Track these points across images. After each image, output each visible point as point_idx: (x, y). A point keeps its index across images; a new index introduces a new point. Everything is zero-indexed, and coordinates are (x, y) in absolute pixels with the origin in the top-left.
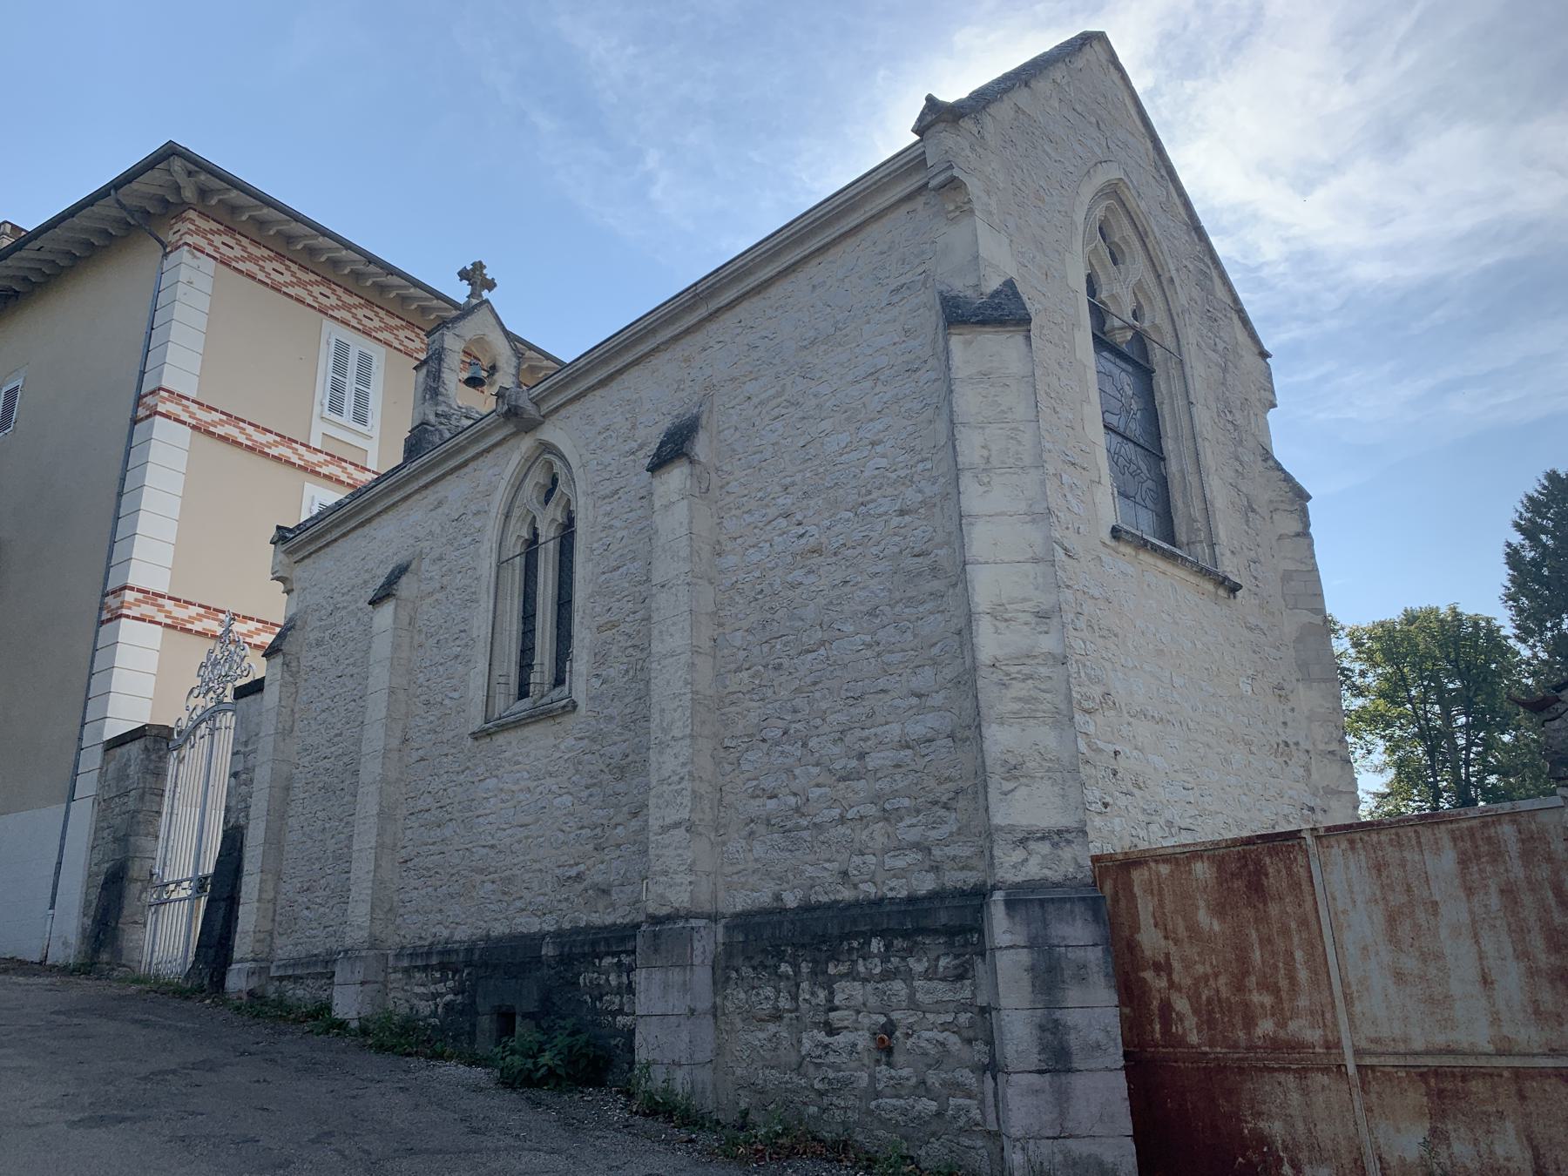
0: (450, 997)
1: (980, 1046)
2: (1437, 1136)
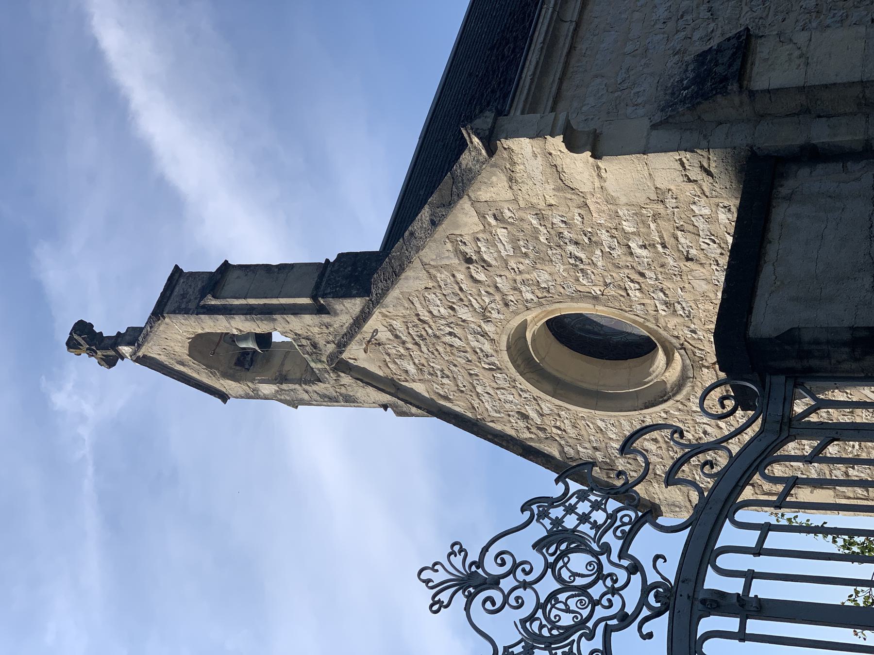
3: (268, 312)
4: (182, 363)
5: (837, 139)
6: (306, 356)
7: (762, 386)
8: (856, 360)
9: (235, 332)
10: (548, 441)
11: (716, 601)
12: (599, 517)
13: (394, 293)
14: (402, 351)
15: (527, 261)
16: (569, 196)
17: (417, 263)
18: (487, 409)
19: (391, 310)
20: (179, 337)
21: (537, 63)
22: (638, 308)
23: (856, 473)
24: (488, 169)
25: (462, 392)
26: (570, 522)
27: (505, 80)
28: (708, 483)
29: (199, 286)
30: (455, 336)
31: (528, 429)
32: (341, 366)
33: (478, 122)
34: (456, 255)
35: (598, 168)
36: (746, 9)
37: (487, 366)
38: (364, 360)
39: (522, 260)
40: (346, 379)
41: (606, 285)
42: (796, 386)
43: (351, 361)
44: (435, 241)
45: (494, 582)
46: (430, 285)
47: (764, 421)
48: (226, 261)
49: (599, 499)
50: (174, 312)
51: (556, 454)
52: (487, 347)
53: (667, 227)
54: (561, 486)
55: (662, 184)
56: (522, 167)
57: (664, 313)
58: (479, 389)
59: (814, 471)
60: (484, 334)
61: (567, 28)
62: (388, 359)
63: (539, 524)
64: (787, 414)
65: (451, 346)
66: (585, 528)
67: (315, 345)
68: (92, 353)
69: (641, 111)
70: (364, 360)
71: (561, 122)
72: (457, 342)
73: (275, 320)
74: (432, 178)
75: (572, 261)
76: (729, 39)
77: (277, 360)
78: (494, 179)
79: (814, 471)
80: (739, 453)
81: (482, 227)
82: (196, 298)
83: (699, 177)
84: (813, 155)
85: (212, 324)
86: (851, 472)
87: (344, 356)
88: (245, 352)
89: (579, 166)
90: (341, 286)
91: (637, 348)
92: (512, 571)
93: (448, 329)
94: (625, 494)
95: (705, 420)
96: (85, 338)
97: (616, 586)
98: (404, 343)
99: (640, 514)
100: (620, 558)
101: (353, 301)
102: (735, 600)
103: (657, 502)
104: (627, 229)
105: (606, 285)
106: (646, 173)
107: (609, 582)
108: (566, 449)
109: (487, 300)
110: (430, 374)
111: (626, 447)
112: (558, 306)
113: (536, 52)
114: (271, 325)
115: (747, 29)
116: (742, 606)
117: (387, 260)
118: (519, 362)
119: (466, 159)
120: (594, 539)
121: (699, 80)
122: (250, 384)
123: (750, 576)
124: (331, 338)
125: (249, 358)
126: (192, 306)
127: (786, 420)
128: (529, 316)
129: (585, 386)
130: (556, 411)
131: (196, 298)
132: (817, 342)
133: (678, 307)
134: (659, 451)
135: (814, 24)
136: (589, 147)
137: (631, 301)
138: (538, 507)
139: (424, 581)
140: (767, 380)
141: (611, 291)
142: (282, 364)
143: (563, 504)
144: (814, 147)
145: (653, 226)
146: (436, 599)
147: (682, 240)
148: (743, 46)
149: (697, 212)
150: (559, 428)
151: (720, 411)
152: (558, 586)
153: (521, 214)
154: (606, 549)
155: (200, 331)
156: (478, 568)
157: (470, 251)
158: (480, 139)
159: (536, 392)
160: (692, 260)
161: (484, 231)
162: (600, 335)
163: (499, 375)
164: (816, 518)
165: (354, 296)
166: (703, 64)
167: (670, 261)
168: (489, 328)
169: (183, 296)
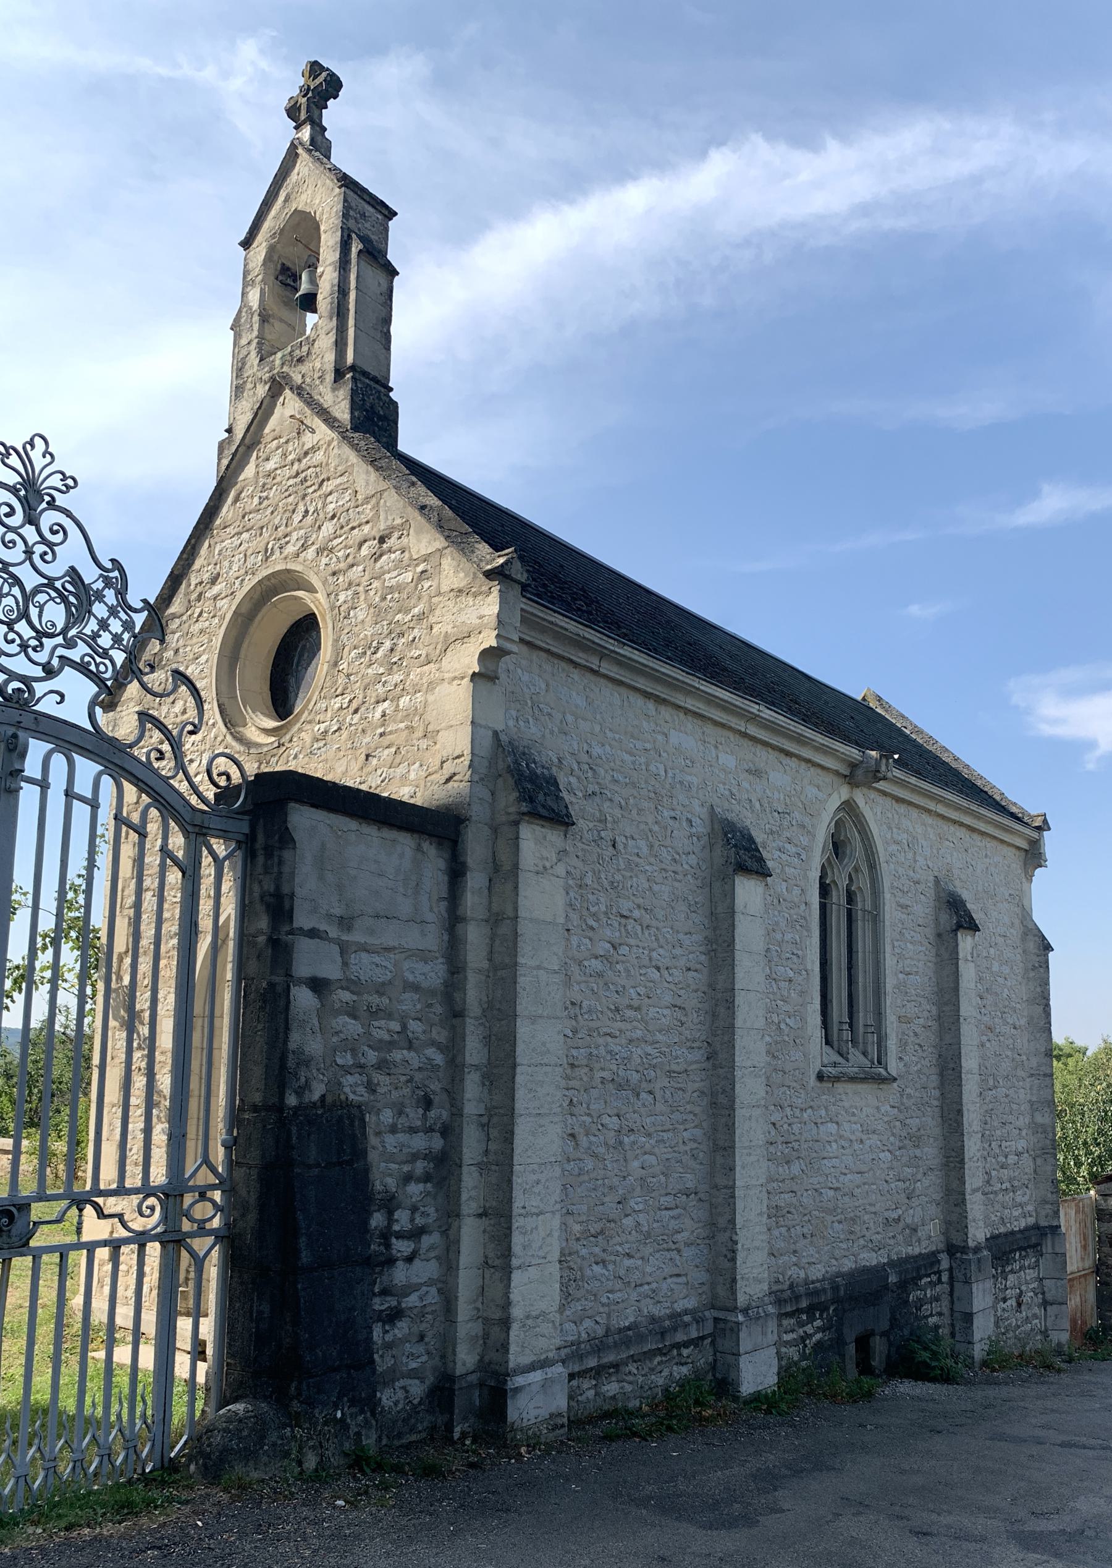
0: (819, 1336)
1: (1040, 1296)
2: (399, 1303)
3: (341, 312)
4: (287, 199)
5: (469, 895)
6: (289, 349)
7: (241, 812)
8: (262, 897)
9: (320, 270)
10: (186, 603)
11: (16, 748)
12: (105, 640)
13: (353, 457)
14: (291, 457)
15: (377, 599)
16: (439, 647)
17: (383, 485)
18: (221, 542)
19: (336, 451)
20: (317, 202)
21: (566, 630)
22: (323, 705)
23: (148, 898)
24: (473, 570)
25: (244, 517)
26: (100, 610)
27: (554, 598)
28: (140, 753)
29: (373, 237)
30: (304, 517)
31: (201, 583)
32: (277, 387)
33: (518, 565)
34: (388, 528)
35: (463, 678)
36: (591, 825)
37: (270, 546)
38: (282, 414)
39: (379, 594)
40: (262, 390)
41: (348, 676)
42: (239, 842)
43: (281, 399)
44: (405, 507)
45: (32, 519)
46: (359, 497)
47: (203, 812)
48: (398, 273)
49: (125, 643)
50: (345, 200)
51: (172, 610)
52: (290, 549)
53: (400, 739)
54: (140, 605)
55: (442, 737)
56: (471, 603)
57: (316, 729)
58: (245, 536)
59: (153, 860)
60: (304, 547)
61: (594, 662)
62: (282, 440)
63: (97, 577)
64: (211, 832)
65: (294, 511)
66: (92, 626)
67: (300, 360)
68: (305, 91)
69: (511, 723)
70: (282, 414)
71: (508, 646)
72: (297, 517)
73: (331, 319)
74: (470, 515)
75: (375, 644)
76: (566, 807)
77: (285, 314)
78: (462, 575)
79: (153, 860)
80: (172, 787)
81: (415, 557)
82: (359, 229)
83: (445, 771)
84: (456, 873)
85: (330, 243)
86: (150, 893)
87: (287, 392)
88: (296, 278)
89: (466, 659)
90: (364, 400)
91: (282, 699)
92: (44, 541)
93: (311, 509)
94: (131, 670)
95: (205, 762)
96: (322, 87)
97: (30, 650)
98: (299, 460)
99: (109, 683)
100: (60, 657)
101: (348, 411)
102: (18, 767)
103: (119, 709)
104: (402, 700)
105: (348, 676)
106: (453, 723)
107: (33, 643)
108: (177, 620)
109: (340, 554)
110: (264, 485)
111: (180, 676)
112: (330, 626)
113: (575, 630)
114: (325, 314)
115: (573, 824)
116: (11, 774)
117: (388, 454)
118: (273, 581)
119: (484, 549)
120: (80, 632)
121: (534, 778)
122: (260, 277)
123: (44, 785)
124: (308, 380)
125: (289, 281)
126: (351, 224)
127: (204, 831)
128: (321, 596)
129: (245, 645)
130: (219, 614)
131: (359, 229)
132: (280, 863)
133: (321, 744)
134: (176, 710)
135: (571, 882)
136: (483, 671)
137: (331, 699)
138: (116, 578)
139: (32, 439)
140: (246, 817)
141: (341, 680)
142: (281, 320)
143: (119, 604)
144: (464, 874)
145: (402, 725)
146: (11, 451)
147: (386, 752)
148: (559, 818)
149: (412, 768)
150: (200, 615)
151: (215, 773)
152: (28, 588)
153: (425, 599)
154: (70, 644)
155: (322, 228)
156: (48, 503)
157: (392, 542)
158: (502, 565)
159: (240, 596)
160: (367, 759)
161: (411, 559)
162: (297, 667)
163: (260, 558)
164: (104, 860)
165: (352, 413)
166: (547, 783)
167: (367, 739)
168: (311, 553)
169: (363, 216)
